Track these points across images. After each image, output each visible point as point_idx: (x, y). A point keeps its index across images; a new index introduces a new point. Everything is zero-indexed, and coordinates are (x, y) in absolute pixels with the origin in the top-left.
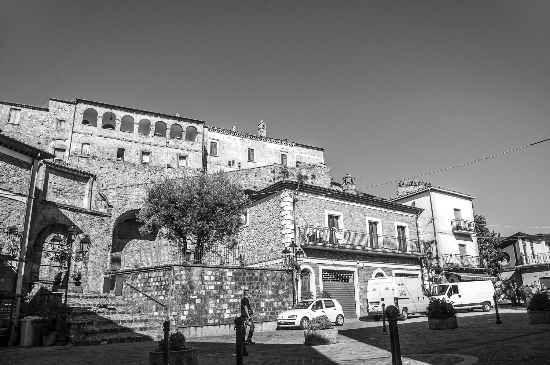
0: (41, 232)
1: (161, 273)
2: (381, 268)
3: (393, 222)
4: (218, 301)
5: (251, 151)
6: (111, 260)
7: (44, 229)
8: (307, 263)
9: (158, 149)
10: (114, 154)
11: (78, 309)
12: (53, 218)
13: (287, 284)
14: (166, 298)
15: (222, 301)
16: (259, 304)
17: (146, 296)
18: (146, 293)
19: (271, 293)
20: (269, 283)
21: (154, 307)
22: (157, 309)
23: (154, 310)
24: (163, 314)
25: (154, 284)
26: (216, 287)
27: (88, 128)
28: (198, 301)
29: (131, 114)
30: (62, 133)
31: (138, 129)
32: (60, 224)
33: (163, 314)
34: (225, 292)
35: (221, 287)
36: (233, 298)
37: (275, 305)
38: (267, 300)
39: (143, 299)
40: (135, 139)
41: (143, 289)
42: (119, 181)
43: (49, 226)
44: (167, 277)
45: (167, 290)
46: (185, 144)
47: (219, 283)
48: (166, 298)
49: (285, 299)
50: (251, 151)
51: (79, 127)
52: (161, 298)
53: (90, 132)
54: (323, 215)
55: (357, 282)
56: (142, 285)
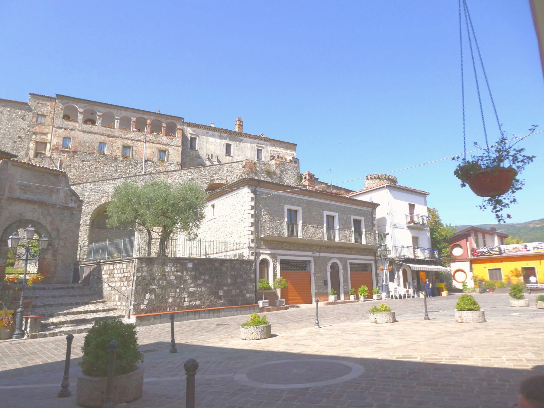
0: (7, 228)
1: (125, 265)
2: (336, 258)
3: (349, 216)
4: (178, 290)
5: (228, 147)
6: (133, 247)
7: (10, 225)
8: (267, 254)
9: (139, 144)
10: (96, 148)
11: (246, 310)
12: (20, 214)
13: (245, 273)
14: (128, 288)
15: (183, 290)
16: (218, 292)
17: (110, 286)
18: (110, 284)
19: (229, 281)
20: (228, 273)
21: (117, 297)
22: (120, 299)
23: (117, 299)
24: (124, 303)
25: (118, 275)
26: (177, 277)
27: (70, 124)
28: (158, 291)
29: (112, 110)
30: (43, 127)
31: (118, 124)
32: (27, 220)
33: (124, 303)
34: (186, 281)
35: (181, 277)
36: (193, 287)
37: (234, 292)
38: (225, 288)
39: (108, 289)
40: (117, 134)
41: (108, 280)
42: (101, 174)
43: (16, 222)
44: (129, 269)
45: (129, 281)
46: (164, 139)
47: (179, 273)
48: (128, 288)
49: (244, 287)
50: (228, 147)
51: (59, 121)
52: (124, 288)
53: (71, 127)
54: (283, 210)
55: (313, 270)
56: (108, 276)
